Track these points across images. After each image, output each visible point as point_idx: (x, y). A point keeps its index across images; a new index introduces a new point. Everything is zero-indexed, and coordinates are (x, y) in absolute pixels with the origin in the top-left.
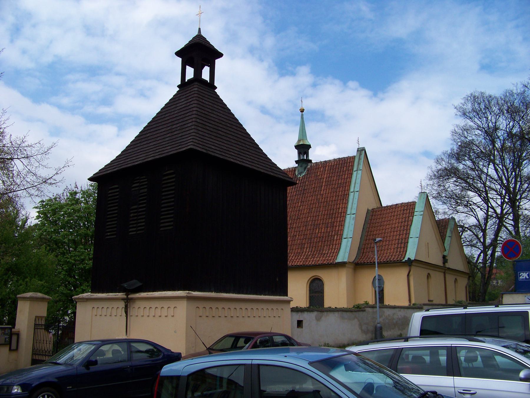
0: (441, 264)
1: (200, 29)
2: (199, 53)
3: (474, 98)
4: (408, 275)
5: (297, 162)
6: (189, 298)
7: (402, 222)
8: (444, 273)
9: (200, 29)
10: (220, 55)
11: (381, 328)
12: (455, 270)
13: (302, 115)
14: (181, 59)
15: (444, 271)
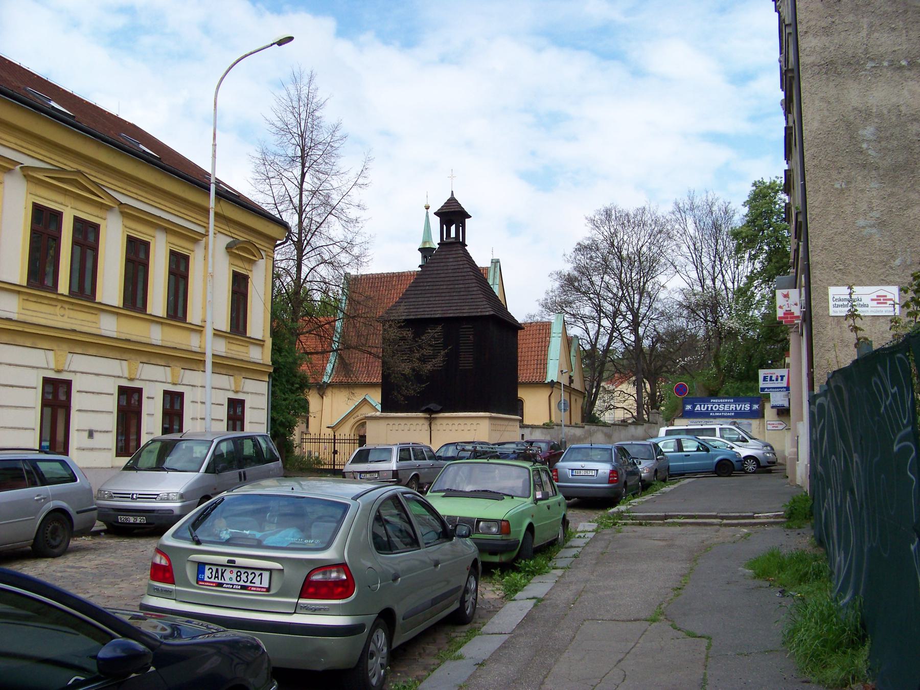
10: (470, 217)
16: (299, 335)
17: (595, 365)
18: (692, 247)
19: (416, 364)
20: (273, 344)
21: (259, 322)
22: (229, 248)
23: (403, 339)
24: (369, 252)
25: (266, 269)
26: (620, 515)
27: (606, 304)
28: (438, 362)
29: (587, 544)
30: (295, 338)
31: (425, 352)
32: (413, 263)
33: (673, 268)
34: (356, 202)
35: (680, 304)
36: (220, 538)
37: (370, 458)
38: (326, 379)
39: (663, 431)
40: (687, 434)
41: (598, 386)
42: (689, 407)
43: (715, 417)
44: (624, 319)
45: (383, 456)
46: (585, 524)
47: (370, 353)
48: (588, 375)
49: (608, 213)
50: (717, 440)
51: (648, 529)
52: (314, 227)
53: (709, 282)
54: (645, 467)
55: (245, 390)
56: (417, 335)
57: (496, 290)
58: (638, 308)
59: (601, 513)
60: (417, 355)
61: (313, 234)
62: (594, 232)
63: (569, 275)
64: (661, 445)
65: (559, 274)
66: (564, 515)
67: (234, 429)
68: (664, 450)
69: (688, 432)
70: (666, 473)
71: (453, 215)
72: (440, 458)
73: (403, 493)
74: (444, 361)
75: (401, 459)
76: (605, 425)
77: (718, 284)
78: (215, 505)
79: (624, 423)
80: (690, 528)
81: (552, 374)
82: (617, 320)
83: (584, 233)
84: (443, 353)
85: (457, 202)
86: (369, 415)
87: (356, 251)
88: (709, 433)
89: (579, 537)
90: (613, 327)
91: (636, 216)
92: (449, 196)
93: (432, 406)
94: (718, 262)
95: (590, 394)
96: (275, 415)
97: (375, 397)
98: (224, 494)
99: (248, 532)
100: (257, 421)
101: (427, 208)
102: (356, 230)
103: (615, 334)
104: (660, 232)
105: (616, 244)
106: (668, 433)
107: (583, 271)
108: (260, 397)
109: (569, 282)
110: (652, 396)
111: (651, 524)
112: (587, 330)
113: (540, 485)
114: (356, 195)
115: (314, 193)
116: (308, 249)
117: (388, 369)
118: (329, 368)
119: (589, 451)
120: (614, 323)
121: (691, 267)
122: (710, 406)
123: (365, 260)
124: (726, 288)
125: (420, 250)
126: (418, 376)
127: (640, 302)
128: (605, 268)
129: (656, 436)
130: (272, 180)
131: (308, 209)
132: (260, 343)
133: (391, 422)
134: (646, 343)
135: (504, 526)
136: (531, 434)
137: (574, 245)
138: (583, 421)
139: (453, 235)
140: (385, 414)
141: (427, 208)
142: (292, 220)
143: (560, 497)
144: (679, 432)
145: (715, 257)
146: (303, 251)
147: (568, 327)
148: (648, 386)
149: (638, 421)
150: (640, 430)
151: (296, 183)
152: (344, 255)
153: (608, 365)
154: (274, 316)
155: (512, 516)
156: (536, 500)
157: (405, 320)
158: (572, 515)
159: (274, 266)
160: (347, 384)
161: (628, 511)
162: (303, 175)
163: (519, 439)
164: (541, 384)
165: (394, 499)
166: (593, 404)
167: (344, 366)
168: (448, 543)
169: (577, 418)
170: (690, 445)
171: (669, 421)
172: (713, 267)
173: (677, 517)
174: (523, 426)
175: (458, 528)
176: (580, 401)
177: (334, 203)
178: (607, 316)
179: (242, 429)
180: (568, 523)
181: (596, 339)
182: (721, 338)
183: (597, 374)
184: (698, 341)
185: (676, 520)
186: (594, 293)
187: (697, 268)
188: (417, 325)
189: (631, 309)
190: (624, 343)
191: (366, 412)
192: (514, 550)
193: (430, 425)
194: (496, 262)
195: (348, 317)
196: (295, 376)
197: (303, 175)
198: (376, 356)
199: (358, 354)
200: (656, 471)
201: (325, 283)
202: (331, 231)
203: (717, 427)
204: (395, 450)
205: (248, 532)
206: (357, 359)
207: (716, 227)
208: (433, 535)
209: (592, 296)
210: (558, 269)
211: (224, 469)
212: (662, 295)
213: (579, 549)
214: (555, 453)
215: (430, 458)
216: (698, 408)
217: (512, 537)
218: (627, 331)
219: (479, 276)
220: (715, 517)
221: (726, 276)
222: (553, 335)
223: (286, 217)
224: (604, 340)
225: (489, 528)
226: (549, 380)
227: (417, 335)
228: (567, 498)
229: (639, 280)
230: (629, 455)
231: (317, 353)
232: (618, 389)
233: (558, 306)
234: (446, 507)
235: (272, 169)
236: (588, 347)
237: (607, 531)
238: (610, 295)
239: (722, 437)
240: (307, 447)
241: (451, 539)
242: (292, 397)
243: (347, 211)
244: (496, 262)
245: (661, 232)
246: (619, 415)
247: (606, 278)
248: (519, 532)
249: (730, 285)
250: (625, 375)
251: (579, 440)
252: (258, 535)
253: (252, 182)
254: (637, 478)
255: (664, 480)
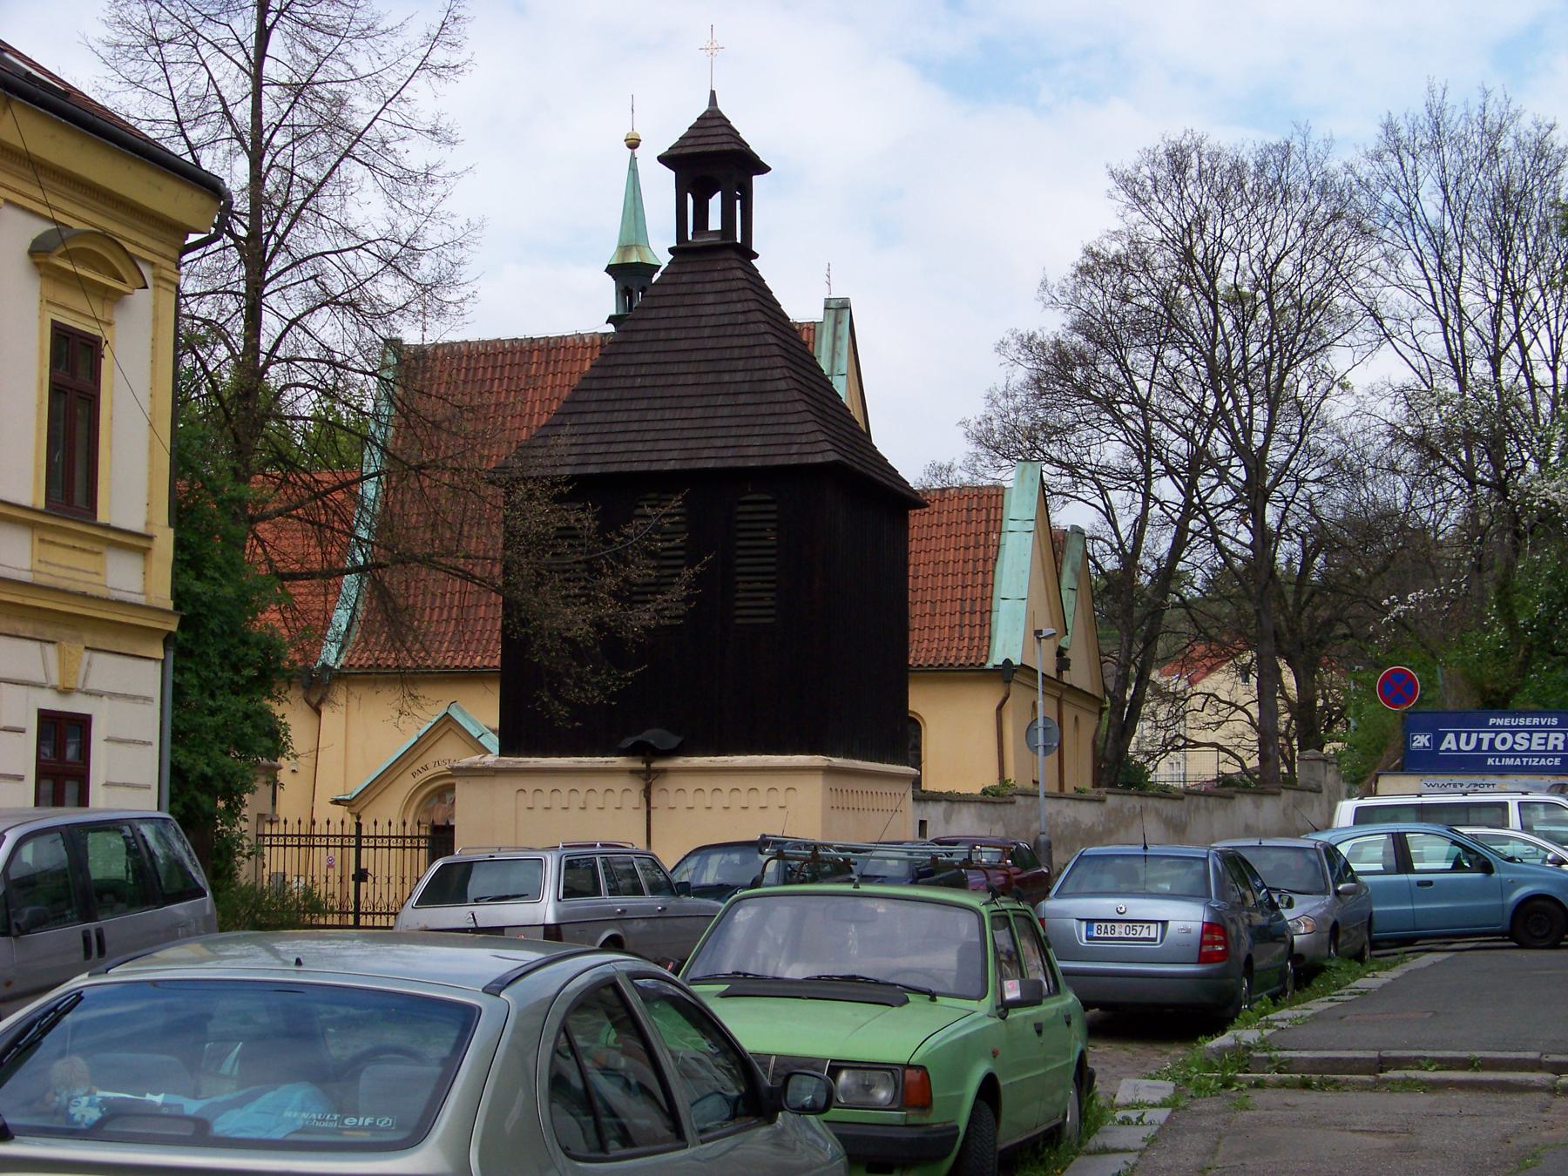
1: (713, 94)
4: (1000, 708)
5: (611, 320)
6: (829, 771)
7: (967, 548)
8: (1059, 702)
9: (713, 94)
10: (764, 169)
11: (1049, 845)
13: (633, 159)
14: (673, 174)
15: (1057, 694)
16: (253, 520)
17: (1132, 618)
18: (1431, 262)
19: (609, 610)
20: (180, 545)
21: (133, 476)
22: (39, 251)
23: (567, 533)
24: (465, 273)
25: (156, 319)
26: (1242, 1057)
27: (1167, 435)
28: (674, 600)
29: (1152, 1141)
30: (243, 527)
31: (634, 573)
32: (585, 307)
33: (1369, 323)
34: (425, 119)
35: (1396, 434)
36: (70, 1117)
37: (473, 889)
38: (330, 654)
39: (1346, 810)
40: (1420, 820)
41: (1143, 679)
42: (1421, 741)
43: (1502, 771)
44: (1223, 476)
45: (514, 881)
46: (1137, 1084)
47: (467, 577)
48: (1111, 647)
49: (1177, 161)
50: (1513, 839)
51: (1329, 1098)
52: (298, 196)
53: (1481, 368)
54: (1303, 916)
55: (93, 685)
56: (610, 522)
57: (840, 386)
58: (1264, 449)
59: (1178, 1052)
60: (610, 582)
61: (296, 217)
62: (1137, 216)
63: (1058, 343)
64: (1344, 849)
65: (1029, 344)
66: (1082, 1055)
67: (58, 800)
68: (1356, 867)
69: (1423, 812)
70: (1364, 937)
71: (714, 164)
72: (685, 889)
73: (633, 976)
74: (687, 600)
75: (570, 892)
76: (1165, 792)
77: (1509, 371)
78: (55, 1015)
79: (1225, 787)
80: (1461, 1097)
81: (1009, 641)
82: (1202, 482)
83: (1103, 220)
84: (687, 573)
85: (725, 123)
86: (465, 761)
87: (426, 268)
88: (1485, 815)
89: (1126, 1121)
90: (1188, 502)
91: (1261, 168)
92: (704, 107)
93: (651, 736)
94: (1508, 306)
95: (1118, 703)
96: (182, 755)
97: (481, 713)
98: (81, 981)
99: (159, 1099)
100: (127, 775)
101: (633, 144)
102: (426, 204)
103: (1193, 524)
104: (1336, 217)
105: (1199, 251)
106: (1362, 816)
107: (1102, 334)
108: (139, 707)
109: (1059, 371)
110: (1304, 711)
111: (1337, 1086)
112: (1109, 514)
113: (1011, 961)
114: (425, 99)
115: (298, 91)
116: (279, 262)
117: (524, 623)
118: (341, 617)
119: (1139, 864)
120: (1189, 489)
121: (1430, 324)
122: (1486, 737)
123: (454, 297)
124: (1532, 384)
125: (611, 270)
126: (611, 646)
127: (1269, 432)
128: (1165, 325)
129: (1328, 826)
130: (169, 49)
131: (279, 140)
132: (136, 543)
133: (529, 784)
134: (1286, 552)
135: (912, 1083)
136: (947, 820)
137: (1077, 256)
138: (1097, 783)
139: (715, 223)
140: (511, 761)
141: (633, 144)
142: (236, 174)
143: (1070, 998)
144: (1393, 813)
145: (1500, 292)
146: (266, 266)
147: (1055, 502)
148: (1289, 679)
149: (1261, 782)
150: (1270, 810)
151: (240, 58)
152: (389, 280)
153: (1170, 616)
154: (182, 462)
155: (935, 1054)
156: (1005, 1007)
157: (572, 479)
158: (1104, 1056)
159: (178, 307)
160: (396, 669)
161: (1265, 1044)
162: (263, 35)
163: (911, 832)
164: (974, 672)
165: (604, 999)
166: (1125, 730)
167: (388, 614)
168: (763, 1131)
169: (1080, 773)
170: (1431, 853)
171: (1361, 782)
172: (1496, 321)
173: (1416, 1063)
174: (923, 797)
175: (793, 1081)
176: (1089, 724)
177: (360, 122)
178: (1170, 471)
179: (83, 800)
180: (1092, 1076)
181: (1138, 537)
182: (1517, 533)
183: (1138, 647)
184: (1440, 545)
185: (1412, 1074)
186: (1132, 401)
187: (1444, 323)
188: (610, 493)
189: (1240, 448)
190: (1222, 550)
191: (450, 754)
192: (946, 1155)
193: (647, 793)
194: (839, 308)
195: (398, 469)
196: (244, 643)
197: (263, 35)
198: (485, 583)
199: (433, 579)
200: (1335, 928)
201: (332, 364)
202: (351, 206)
203: (1513, 801)
204: (552, 863)
205: (159, 1099)
206: (433, 596)
207: (1508, 200)
208: (713, 1105)
209: (1125, 408)
210: (1026, 329)
211: (38, 923)
212: (1337, 408)
213: (1132, 1158)
214: (1024, 877)
215: (656, 889)
216: (1449, 742)
217: (935, 1118)
218: (1229, 514)
219: (793, 343)
220: (1536, 1066)
221: (1535, 352)
222: (1009, 525)
223: (209, 161)
224: (1160, 542)
225: (867, 1088)
226: (997, 659)
227: (610, 522)
228: (1087, 1005)
229: (1266, 364)
230: (1255, 875)
231: (310, 575)
232: (1199, 688)
233: (1021, 441)
234: (762, 1029)
235: (165, 15)
236: (1111, 563)
237: (1205, 1104)
238: (1183, 408)
239: (1526, 828)
240: (279, 861)
241: (771, 1120)
242: (240, 704)
243: (399, 146)
244: (839, 308)
245: (1341, 215)
246: (1203, 766)
247: (1171, 356)
248: (956, 1105)
249: (1543, 375)
250: (1223, 645)
251: (1092, 837)
252: (192, 1107)
253: (107, 52)
254: (1281, 948)
255: (1359, 957)
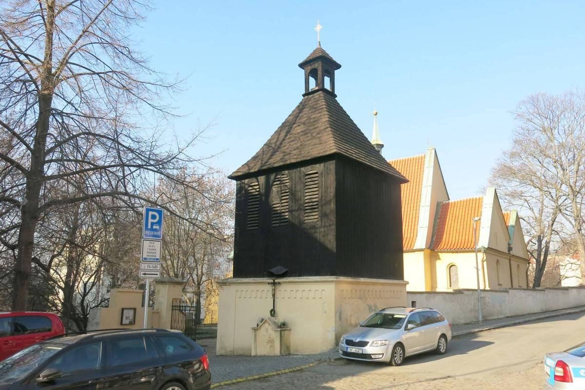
0: (506, 251)
2: (321, 66)
3: (534, 101)
6: (337, 282)
8: (510, 260)
10: (338, 66)
12: (499, 251)
